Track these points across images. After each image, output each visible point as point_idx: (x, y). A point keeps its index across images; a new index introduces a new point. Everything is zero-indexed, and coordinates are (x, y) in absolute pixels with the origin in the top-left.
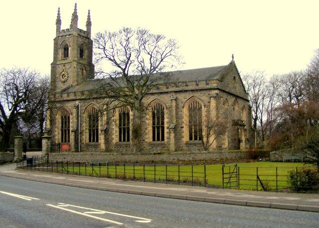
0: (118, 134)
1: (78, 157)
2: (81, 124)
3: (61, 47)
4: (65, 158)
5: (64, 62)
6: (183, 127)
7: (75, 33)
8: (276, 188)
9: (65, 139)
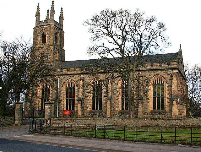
0: (91, 103)
6: (148, 99)
8: (35, 129)
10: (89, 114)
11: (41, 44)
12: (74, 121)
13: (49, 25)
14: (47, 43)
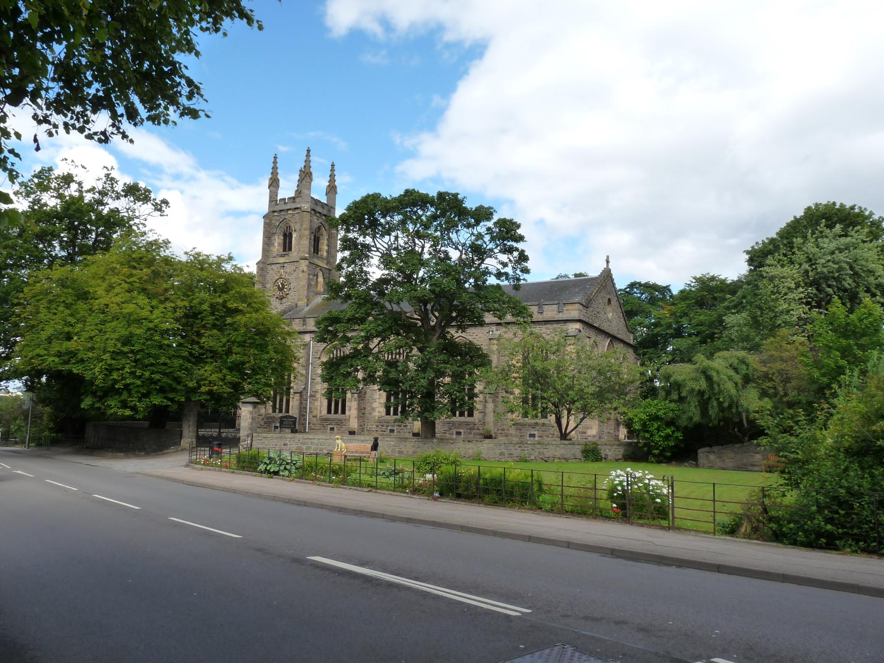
1: (311, 443)
2: (312, 379)
3: (480, 209)
4: (285, 445)
5: (282, 260)
7: (306, 206)
9: (281, 405)
10: (377, 426)
11: (282, 256)
12: (299, 440)
13: (298, 208)
14: (294, 254)
